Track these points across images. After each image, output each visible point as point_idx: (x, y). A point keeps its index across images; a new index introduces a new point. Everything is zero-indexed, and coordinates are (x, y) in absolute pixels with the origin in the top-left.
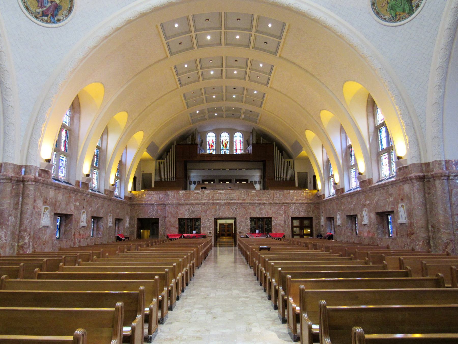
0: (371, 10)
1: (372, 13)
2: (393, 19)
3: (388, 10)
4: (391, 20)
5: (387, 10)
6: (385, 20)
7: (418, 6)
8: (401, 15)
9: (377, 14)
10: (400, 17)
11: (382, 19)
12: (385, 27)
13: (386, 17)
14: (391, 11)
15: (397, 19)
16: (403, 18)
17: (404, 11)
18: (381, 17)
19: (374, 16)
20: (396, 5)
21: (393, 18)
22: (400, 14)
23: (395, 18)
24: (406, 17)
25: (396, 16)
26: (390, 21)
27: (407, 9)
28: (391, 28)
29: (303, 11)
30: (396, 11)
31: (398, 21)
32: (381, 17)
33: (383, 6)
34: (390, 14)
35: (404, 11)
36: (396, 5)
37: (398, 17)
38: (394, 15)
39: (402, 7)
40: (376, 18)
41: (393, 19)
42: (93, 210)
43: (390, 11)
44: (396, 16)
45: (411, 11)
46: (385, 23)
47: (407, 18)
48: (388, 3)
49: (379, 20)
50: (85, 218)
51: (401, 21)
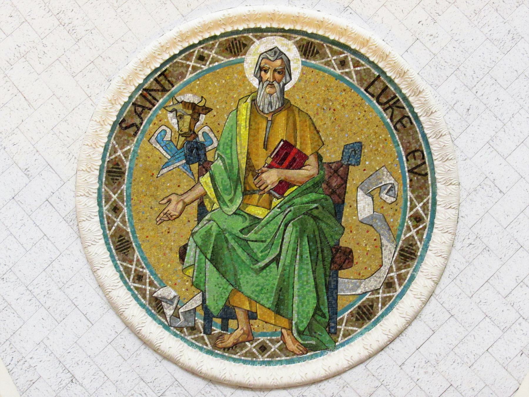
0: (93, 203)
1: (93, 228)
2: (208, 330)
3: (191, 252)
4: (193, 329)
5: (183, 253)
6: (157, 306)
7: (365, 315)
8: (256, 324)
9: (121, 246)
10: (250, 336)
11: (138, 294)
12: (147, 357)
13: (168, 292)
14: (209, 266)
15: (230, 341)
16: (263, 348)
17: (280, 307)
18: (140, 278)
19: (101, 252)
20: (245, 243)
21: (208, 317)
22: (251, 316)
23: (216, 327)
24: (284, 349)
25: (228, 314)
26: (185, 329)
27: (303, 302)
28: (180, 375)
29: (191, 366)
30: (237, 288)
31: (231, 350)
32: (140, 278)
33: (171, 218)
34: (198, 285)
35: (280, 307)
36: (245, 243)
37: (238, 329)
38: (216, 305)
39: (274, 275)
40: (110, 274)
41: (208, 330)
42: (200, 243)
43: (201, 270)
44: (228, 314)
45: (322, 330)
46: (152, 329)
47: (288, 355)
48: (202, 212)
49: (122, 295)
50: (360, 205)
51: (250, 359)
